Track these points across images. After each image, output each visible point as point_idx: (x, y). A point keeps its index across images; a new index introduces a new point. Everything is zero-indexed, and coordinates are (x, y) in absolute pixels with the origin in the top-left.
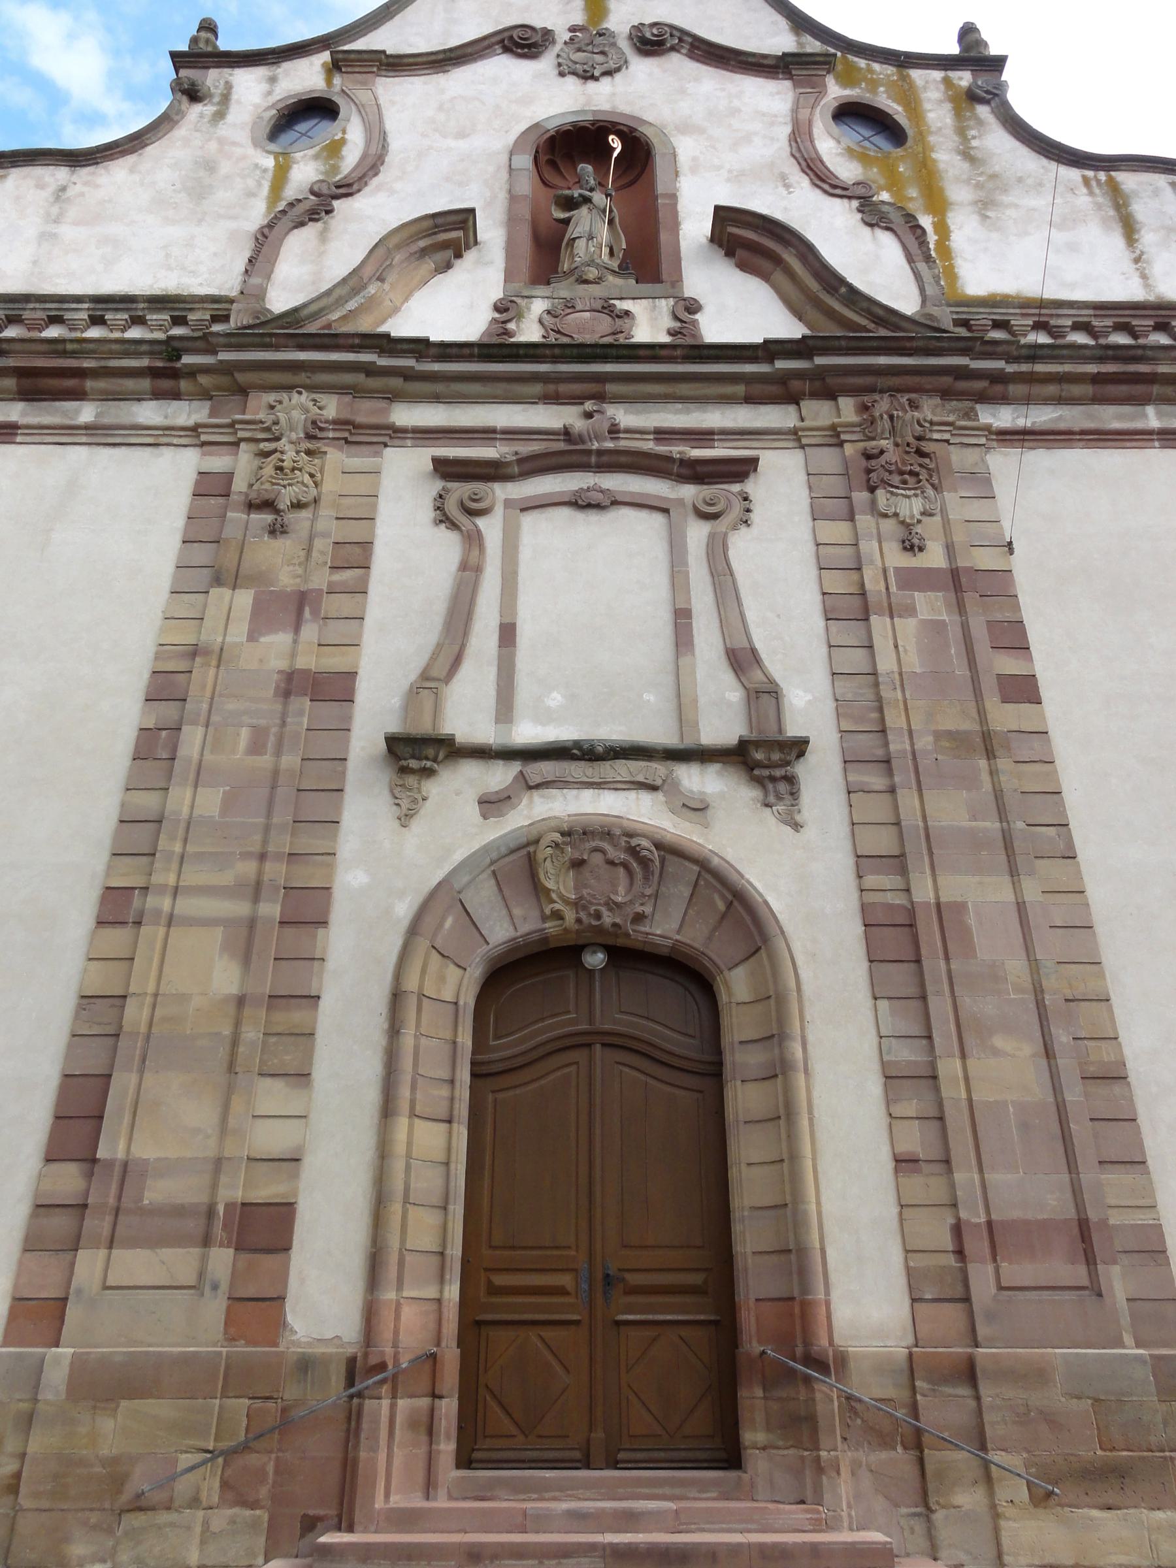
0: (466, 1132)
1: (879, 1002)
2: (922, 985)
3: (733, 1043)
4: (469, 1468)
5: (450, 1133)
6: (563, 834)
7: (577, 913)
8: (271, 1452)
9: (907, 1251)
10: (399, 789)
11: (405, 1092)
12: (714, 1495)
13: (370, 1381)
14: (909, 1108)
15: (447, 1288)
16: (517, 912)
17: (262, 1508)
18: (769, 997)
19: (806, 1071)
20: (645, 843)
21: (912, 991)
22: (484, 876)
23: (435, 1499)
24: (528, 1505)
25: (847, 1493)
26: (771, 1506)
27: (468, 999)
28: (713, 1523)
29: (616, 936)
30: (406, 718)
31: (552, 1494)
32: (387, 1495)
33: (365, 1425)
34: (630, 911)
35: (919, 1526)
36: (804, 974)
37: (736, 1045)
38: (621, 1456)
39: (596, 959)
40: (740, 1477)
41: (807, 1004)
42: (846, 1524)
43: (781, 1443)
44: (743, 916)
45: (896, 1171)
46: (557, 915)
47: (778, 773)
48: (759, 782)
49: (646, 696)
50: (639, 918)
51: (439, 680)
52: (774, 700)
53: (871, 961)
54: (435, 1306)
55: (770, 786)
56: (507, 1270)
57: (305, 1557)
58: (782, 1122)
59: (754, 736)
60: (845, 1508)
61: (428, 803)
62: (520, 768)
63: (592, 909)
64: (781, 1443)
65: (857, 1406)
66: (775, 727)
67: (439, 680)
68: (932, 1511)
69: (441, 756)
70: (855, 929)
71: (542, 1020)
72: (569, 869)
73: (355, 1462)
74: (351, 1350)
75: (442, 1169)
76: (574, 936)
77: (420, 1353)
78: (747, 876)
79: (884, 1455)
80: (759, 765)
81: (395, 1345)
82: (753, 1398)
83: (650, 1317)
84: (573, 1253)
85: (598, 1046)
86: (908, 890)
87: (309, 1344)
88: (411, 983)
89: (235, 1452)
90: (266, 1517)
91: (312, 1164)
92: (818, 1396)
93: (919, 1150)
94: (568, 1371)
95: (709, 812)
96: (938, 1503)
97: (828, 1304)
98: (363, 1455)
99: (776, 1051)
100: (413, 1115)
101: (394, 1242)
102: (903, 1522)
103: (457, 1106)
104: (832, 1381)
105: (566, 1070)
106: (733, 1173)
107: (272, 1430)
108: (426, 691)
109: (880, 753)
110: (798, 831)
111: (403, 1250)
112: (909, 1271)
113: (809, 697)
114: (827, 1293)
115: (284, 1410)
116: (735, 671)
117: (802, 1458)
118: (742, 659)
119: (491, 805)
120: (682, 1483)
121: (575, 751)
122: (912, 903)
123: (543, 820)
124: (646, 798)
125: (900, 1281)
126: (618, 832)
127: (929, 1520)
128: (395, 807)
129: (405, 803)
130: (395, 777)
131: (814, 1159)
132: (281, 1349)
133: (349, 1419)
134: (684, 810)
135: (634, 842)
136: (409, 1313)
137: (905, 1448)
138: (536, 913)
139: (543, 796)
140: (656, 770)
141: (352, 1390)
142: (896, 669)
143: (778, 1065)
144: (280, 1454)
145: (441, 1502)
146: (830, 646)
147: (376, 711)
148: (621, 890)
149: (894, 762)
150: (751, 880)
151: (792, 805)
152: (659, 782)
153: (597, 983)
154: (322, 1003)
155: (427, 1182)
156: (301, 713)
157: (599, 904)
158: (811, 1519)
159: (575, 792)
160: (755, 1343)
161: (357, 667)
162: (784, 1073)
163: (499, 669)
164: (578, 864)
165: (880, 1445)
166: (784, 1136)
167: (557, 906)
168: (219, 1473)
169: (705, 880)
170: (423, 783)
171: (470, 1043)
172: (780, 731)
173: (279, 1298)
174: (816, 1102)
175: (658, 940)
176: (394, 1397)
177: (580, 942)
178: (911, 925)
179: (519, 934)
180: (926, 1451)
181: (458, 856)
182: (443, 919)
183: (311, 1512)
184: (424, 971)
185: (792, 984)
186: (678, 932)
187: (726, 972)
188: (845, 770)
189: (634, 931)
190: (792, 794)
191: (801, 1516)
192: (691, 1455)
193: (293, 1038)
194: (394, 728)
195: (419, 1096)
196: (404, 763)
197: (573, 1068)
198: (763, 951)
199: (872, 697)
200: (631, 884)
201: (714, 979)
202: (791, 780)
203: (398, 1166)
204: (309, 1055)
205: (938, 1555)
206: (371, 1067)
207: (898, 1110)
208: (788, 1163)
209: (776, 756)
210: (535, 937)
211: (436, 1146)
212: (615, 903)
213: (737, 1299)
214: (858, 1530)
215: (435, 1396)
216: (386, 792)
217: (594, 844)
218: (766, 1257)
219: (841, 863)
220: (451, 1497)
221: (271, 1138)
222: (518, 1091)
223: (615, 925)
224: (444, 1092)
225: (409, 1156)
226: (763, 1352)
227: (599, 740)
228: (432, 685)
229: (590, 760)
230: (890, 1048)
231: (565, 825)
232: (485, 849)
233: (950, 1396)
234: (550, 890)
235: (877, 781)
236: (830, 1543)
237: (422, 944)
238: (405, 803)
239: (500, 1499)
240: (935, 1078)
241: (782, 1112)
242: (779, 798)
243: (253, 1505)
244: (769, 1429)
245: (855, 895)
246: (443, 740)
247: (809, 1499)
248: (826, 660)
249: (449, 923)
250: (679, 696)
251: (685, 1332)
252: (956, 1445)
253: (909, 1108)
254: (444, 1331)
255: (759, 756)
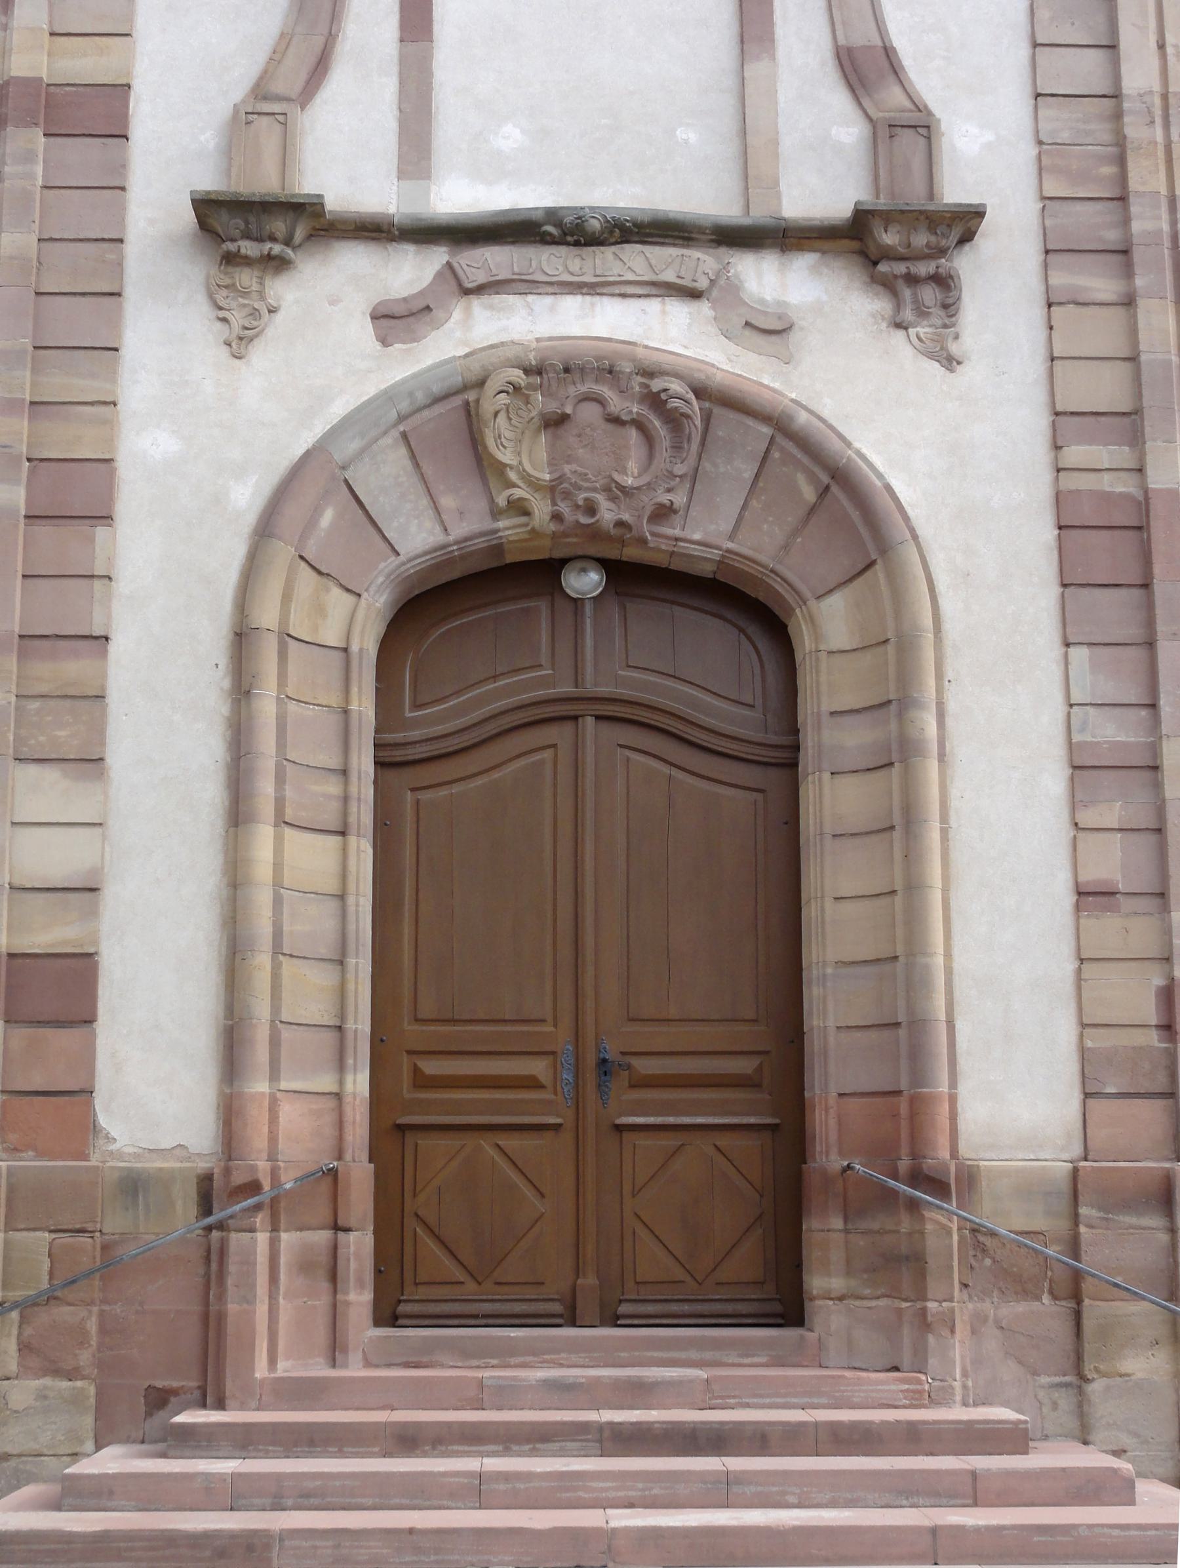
0: (370, 851)
1: (1072, 651)
2: (1150, 623)
3: (819, 714)
4: (395, 1326)
5: (344, 850)
6: (527, 371)
7: (554, 504)
8: (92, 1303)
9: (1083, 1026)
10: (224, 292)
11: (266, 787)
12: (763, 1360)
13: (237, 1208)
14: (1110, 814)
15: (349, 1078)
16: (447, 502)
17: (83, 1378)
18: (886, 641)
19: (942, 756)
20: (676, 386)
21: (1133, 632)
22: (388, 440)
23: (345, 1366)
24: (487, 1373)
25: (963, 1357)
26: (848, 1374)
27: (367, 643)
28: (761, 1396)
29: (623, 542)
30: (230, 166)
31: (521, 1359)
32: (272, 1362)
33: (232, 1268)
34: (647, 502)
35: (1066, 1401)
36: (948, 605)
37: (825, 718)
38: (623, 1309)
39: (585, 582)
40: (802, 1337)
41: (949, 652)
42: (958, 1398)
43: (867, 1292)
44: (847, 509)
45: (1078, 908)
46: (519, 508)
47: (923, 269)
48: (887, 285)
49: (681, 133)
50: (663, 513)
51: (288, 100)
52: (922, 142)
53: (1064, 586)
54: (331, 1103)
55: (907, 293)
56: (441, 1053)
57: (156, 1442)
58: (897, 834)
59: (883, 203)
60: (958, 1377)
61: (279, 318)
62: (445, 258)
63: (581, 497)
64: (867, 1292)
65: (987, 1241)
66: (920, 187)
67: (288, 100)
68: (1087, 1381)
69: (299, 234)
70: (1039, 535)
71: (495, 678)
72: (538, 431)
73: (221, 1317)
74: (203, 1165)
75: (332, 905)
76: (547, 542)
77: (313, 1167)
78: (857, 445)
79: (1022, 1307)
80: (889, 255)
81: (272, 1157)
82: (825, 1231)
83: (671, 1120)
84: (548, 1028)
85: (590, 720)
86: (1140, 470)
87: (136, 1156)
88: (267, 616)
89: (36, 1304)
90: (92, 1390)
91: (118, 896)
92: (929, 1227)
93: (1119, 877)
94: (542, 1195)
95: (795, 336)
96: (1097, 1370)
97: (953, 1099)
98: (232, 1307)
99: (893, 726)
100: (281, 821)
101: (261, 1009)
102: (1041, 1394)
103: (353, 808)
104: (953, 1207)
105: (536, 757)
106: (810, 913)
107: (89, 1274)
108: (265, 120)
109: (1112, 237)
110: (952, 371)
111: (276, 1023)
112: (1084, 1054)
113: (989, 136)
114: (953, 1084)
115: (105, 1248)
116: (852, 90)
117: (899, 1312)
118: (866, 67)
119: (395, 320)
120: (717, 1345)
121: (549, 228)
122: (1146, 492)
123: (492, 347)
124: (679, 312)
125: (1069, 1068)
126: (627, 367)
127: (1080, 1391)
128: (219, 324)
129: (237, 318)
130: (214, 270)
131: (946, 890)
132: (94, 1162)
133: (208, 1259)
134: (748, 332)
135: (656, 385)
136: (289, 1112)
137: (1055, 1297)
138: (482, 505)
139: (491, 307)
140: (700, 263)
141: (210, 1220)
142: (1157, 87)
143: (894, 747)
144: (106, 1308)
145: (354, 1370)
146: (1035, 45)
147: (171, 154)
148: (633, 466)
149: (1138, 254)
150: (864, 451)
151: (945, 326)
152: (702, 284)
153: (588, 621)
154: (113, 648)
155: (312, 924)
156: (29, 157)
157: (595, 490)
158: (907, 1391)
159: (549, 300)
160: (834, 1156)
161: (129, 74)
162: (904, 760)
163: (402, 82)
164: (555, 422)
165: (1016, 1293)
166: (898, 855)
167: (518, 493)
168: (15, 1332)
169: (782, 450)
170: (268, 282)
171: (371, 714)
172: (931, 196)
173: (82, 1091)
174: (954, 803)
175: (696, 550)
176: (275, 1228)
177: (558, 554)
178: (1139, 528)
179: (451, 538)
180: (1087, 1302)
181: (339, 409)
182: (317, 512)
183: (159, 1384)
184: (287, 598)
185: (927, 621)
186: (731, 538)
187: (812, 603)
188: (1046, 266)
189: (653, 534)
190: (945, 307)
191: (893, 1387)
192: (729, 1308)
193: (68, 703)
194: (209, 181)
195: (289, 792)
196: (231, 247)
197: (547, 754)
198: (878, 567)
199: (1107, 137)
200: (651, 456)
201: (790, 611)
202: (944, 282)
203: (262, 898)
204: (98, 729)
205: (1091, 1438)
206: (207, 750)
207: (1088, 817)
208: (902, 898)
209: (921, 239)
210: (480, 543)
211: (321, 871)
212: (622, 488)
213: (807, 1094)
214: (975, 1405)
215: (337, 1228)
216: (201, 298)
217: (583, 388)
218: (858, 1034)
219: (1028, 424)
220: (368, 1364)
221: (49, 857)
222: (456, 789)
223: (620, 524)
224: (333, 787)
225: (278, 884)
226: (849, 1167)
227: (592, 208)
228: (276, 107)
229: (577, 244)
230: (1085, 723)
231: (532, 356)
232: (388, 396)
233: (1131, 1227)
234: (505, 465)
235: (1101, 284)
236: (935, 1422)
237: (282, 553)
238: (237, 318)
239: (442, 1366)
240: (1155, 768)
241: (897, 819)
242: (922, 312)
243: (71, 1375)
244: (849, 1272)
245: (1047, 476)
246: (303, 204)
247: (906, 1362)
248: (1026, 71)
249: (327, 517)
250: (743, 132)
251: (724, 1141)
252: (1136, 1293)
253: (1110, 814)
254: (349, 1138)
255: (889, 238)
